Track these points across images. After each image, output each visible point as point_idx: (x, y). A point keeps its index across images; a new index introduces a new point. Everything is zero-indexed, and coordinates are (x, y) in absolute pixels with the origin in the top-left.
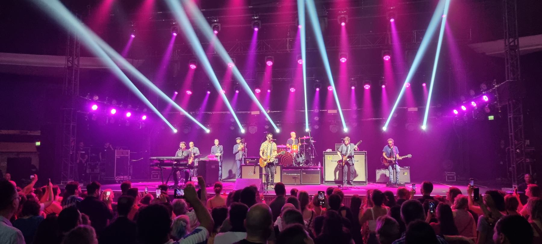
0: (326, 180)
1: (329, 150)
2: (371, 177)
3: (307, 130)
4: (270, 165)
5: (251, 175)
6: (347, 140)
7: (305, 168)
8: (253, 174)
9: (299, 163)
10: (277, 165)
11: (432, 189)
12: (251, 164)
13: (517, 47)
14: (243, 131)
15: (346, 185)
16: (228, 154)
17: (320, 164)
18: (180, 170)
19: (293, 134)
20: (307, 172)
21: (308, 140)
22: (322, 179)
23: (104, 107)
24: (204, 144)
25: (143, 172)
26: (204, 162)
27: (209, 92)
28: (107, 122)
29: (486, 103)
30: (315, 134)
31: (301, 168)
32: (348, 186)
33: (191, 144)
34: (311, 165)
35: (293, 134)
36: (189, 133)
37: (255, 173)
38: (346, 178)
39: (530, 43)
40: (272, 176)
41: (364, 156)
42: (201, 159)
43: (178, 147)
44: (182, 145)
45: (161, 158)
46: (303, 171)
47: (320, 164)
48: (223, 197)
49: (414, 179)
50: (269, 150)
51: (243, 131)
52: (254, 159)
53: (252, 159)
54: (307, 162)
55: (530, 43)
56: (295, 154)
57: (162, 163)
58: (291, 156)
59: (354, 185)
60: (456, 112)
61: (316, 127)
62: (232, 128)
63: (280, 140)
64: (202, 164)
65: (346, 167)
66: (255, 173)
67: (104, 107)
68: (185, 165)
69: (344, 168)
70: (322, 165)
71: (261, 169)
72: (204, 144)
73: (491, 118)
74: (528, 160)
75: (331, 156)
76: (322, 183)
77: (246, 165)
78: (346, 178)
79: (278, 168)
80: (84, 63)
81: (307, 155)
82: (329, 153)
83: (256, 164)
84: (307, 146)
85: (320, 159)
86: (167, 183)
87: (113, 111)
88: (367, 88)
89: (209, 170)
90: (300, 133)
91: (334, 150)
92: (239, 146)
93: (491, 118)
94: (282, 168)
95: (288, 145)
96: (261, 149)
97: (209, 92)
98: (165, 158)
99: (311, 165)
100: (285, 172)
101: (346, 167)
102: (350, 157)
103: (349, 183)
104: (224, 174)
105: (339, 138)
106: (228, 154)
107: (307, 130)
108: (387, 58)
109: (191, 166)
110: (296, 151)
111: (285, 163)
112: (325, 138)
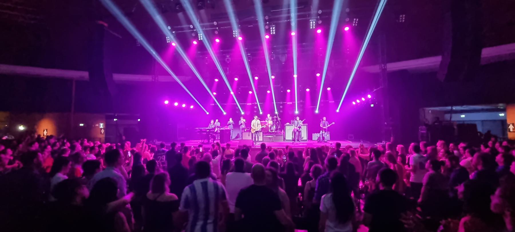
1: (288, 124)
2: (310, 137)
3: (276, 113)
4: (257, 132)
5: (247, 137)
6: (298, 118)
9: (272, 131)
10: (261, 131)
12: (247, 131)
13: (386, 69)
14: (243, 113)
15: (296, 142)
16: (236, 125)
18: (211, 135)
19: (269, 115)
21: (277, 119)
22: (284, 139)
23: (180, 104)
24: (224, 121)
25: (193, 136)
26: (222, 130)
28: (424, 132)
29: (370, 99)
30: (280, 115)
32: (298, 142)
33: (217, 120)
34: (278, 131)
35: (269, 115)
36: (216, 114)
38: (297, 138)
39: (392, 67)
40: (258, 138)
41: (306, 127)
42: (221, 129)
43: (210, 122)
44: (212, 122)
45: (201, 128)
48: (232, 151)
49: (332, 138)
50: (256, 124)
51: (243, 113)
54: (276, 130)
55: (392, 67)
57: (201, 131)
59: (301, 142)
61: (281, 111)
62: (237, 112)
63: (262, 118)
64: (222, 131)
65: (297, 133)
67: (180, 104)
68: (213, 132)
69: (297, 133)
71: (252, 134)
72: (224, 121)
73: (372, 105)
74: (391, 128)
78: (297, 138)
79: (261, 133)
80: (162, 79)
81: (277, 126)
82: (288, 125)
83: (250, 131)
84: (276, 122)
85: (283, 128)
87: (166, 102)
89: (225, 135)
90: (273, 115)
91: (290, 123)
92: (243, 120)
93: (372, 105)
94: (263, 133)
96: (252, 124)
98: (203, 128)
99: (278, 131)
101: (297, 133)
102: (300, 127)
103: (298, 140)
104: (233, 135)
105: (293, 117)
106: (236, 125)
107: (276, 113)
109: (216, 133)
111: (265, 131)
112: (286, 118)
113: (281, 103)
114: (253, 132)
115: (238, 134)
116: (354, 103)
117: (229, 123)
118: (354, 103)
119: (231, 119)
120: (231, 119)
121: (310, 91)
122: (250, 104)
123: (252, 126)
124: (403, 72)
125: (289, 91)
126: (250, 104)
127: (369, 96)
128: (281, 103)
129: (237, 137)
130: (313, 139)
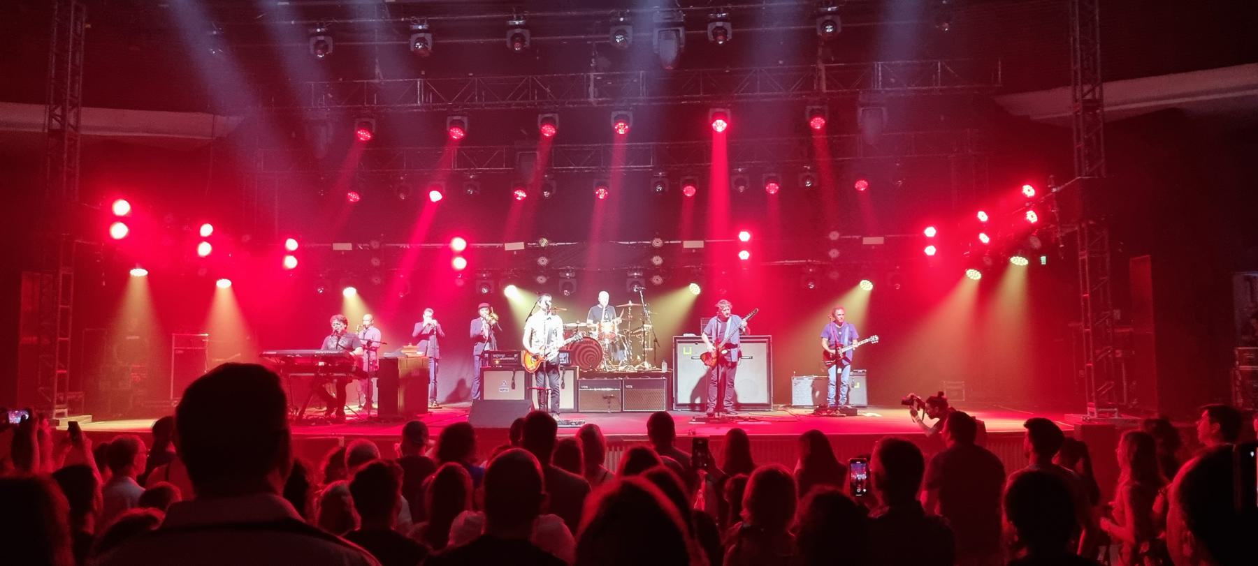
0: (680, 401)
2: (781, 393)
5: (505, 390)
7: (630, 375)
8: (509, 388)
12: (506, 367)
37: (513, 386)
45: (290, 352)
46: (628, 383)
66: (513, 386)
70: (670, 366)
76: (670, 406)
79: (569, 377)
95: (590, 321)
100: (584, 383)
113: (657, 243)
114: (531, 365)
115: (461, 383)
116: (204, 249)
117: (417, 328)
118: (930, 251)
119: (428, 315)
120: (428, 315)
121: (727, 130)
122: (520, 246)
123: (525, 342)
124: (1168, 119)
125: (689, 191)
126: (520, 246)
127: (930, 232)
128: (657, 243)
129: (454, 397)
130: (795, 402)
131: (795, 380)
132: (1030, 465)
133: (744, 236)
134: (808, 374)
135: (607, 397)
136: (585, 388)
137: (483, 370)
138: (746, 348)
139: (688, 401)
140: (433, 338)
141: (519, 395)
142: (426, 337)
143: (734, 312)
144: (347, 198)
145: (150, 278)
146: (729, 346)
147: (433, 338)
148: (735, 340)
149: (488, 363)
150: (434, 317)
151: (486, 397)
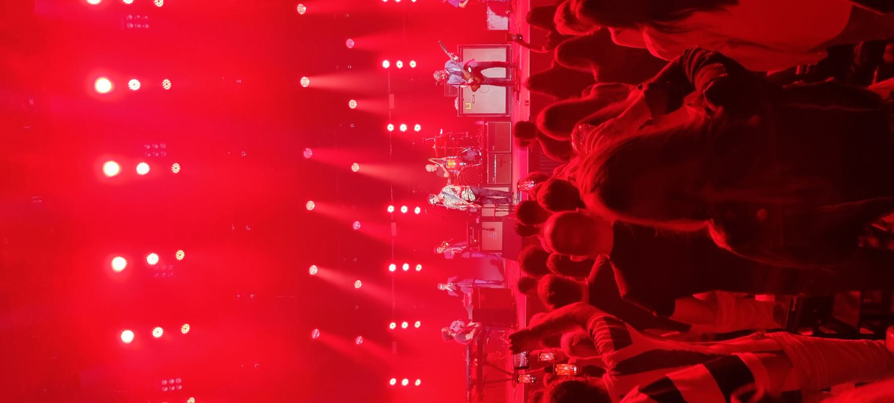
0: (504, 111)
5: (495, 235)
7: (485, 147)
8: (494, 233)
9: (477, 157)
11: (498, 14)
17: (481, 123)
20: (492, 142)
27: (316, 334)
31: (484, 154)
37: (493, 230)
42: (470, 317)
46: (490, 149)
47: (481, 123)
52: (470, 231)
53: (470, 234)
56: (461, 164)
58: (465, 170)
60: (413, 64)
66: (493, 230)
70: (480, 119)
75: (466, 103)
77: (480, 243)
81: (466, 143)
86: (509, 374)
88: (353, 43)
97: (316, 334)
100: (491, 180)
108: (353, 104)
110: (457, 162)
131: (490, 28)
132: (526, 118)
133: (386, 64)
134: (485, 17)
135: (500, 164)
136: (494, 179)
137: (482, 252)
138: (466, 59)
139: (504, 69)
140: (459, 284)
141: (499, 226)
142: (458, 288)
143: (442, 68)
144: (360, 345)
145: (318, 265)
146: (466, 68)
147: (459, 284)
148: (462, 64)
149: (477, 246)
150: (446, 283)
151: (501, 249)
